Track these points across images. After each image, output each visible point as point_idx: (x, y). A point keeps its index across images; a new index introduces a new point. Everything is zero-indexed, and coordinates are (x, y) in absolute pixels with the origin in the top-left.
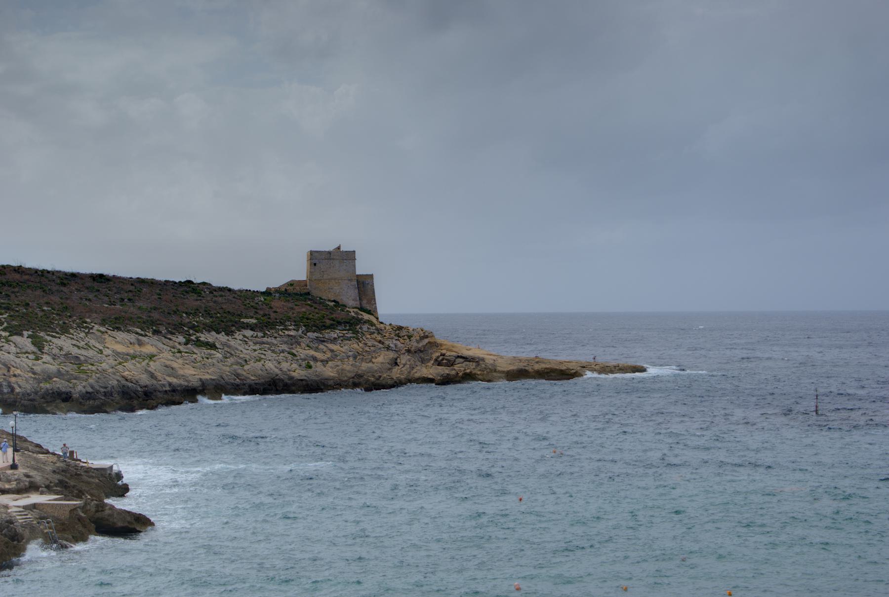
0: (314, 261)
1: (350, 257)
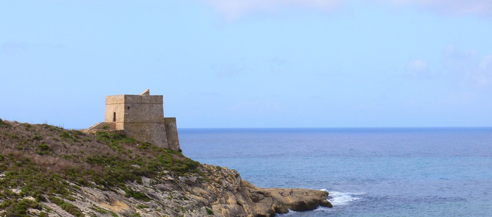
0: (129, 105)
1: (159, 100)
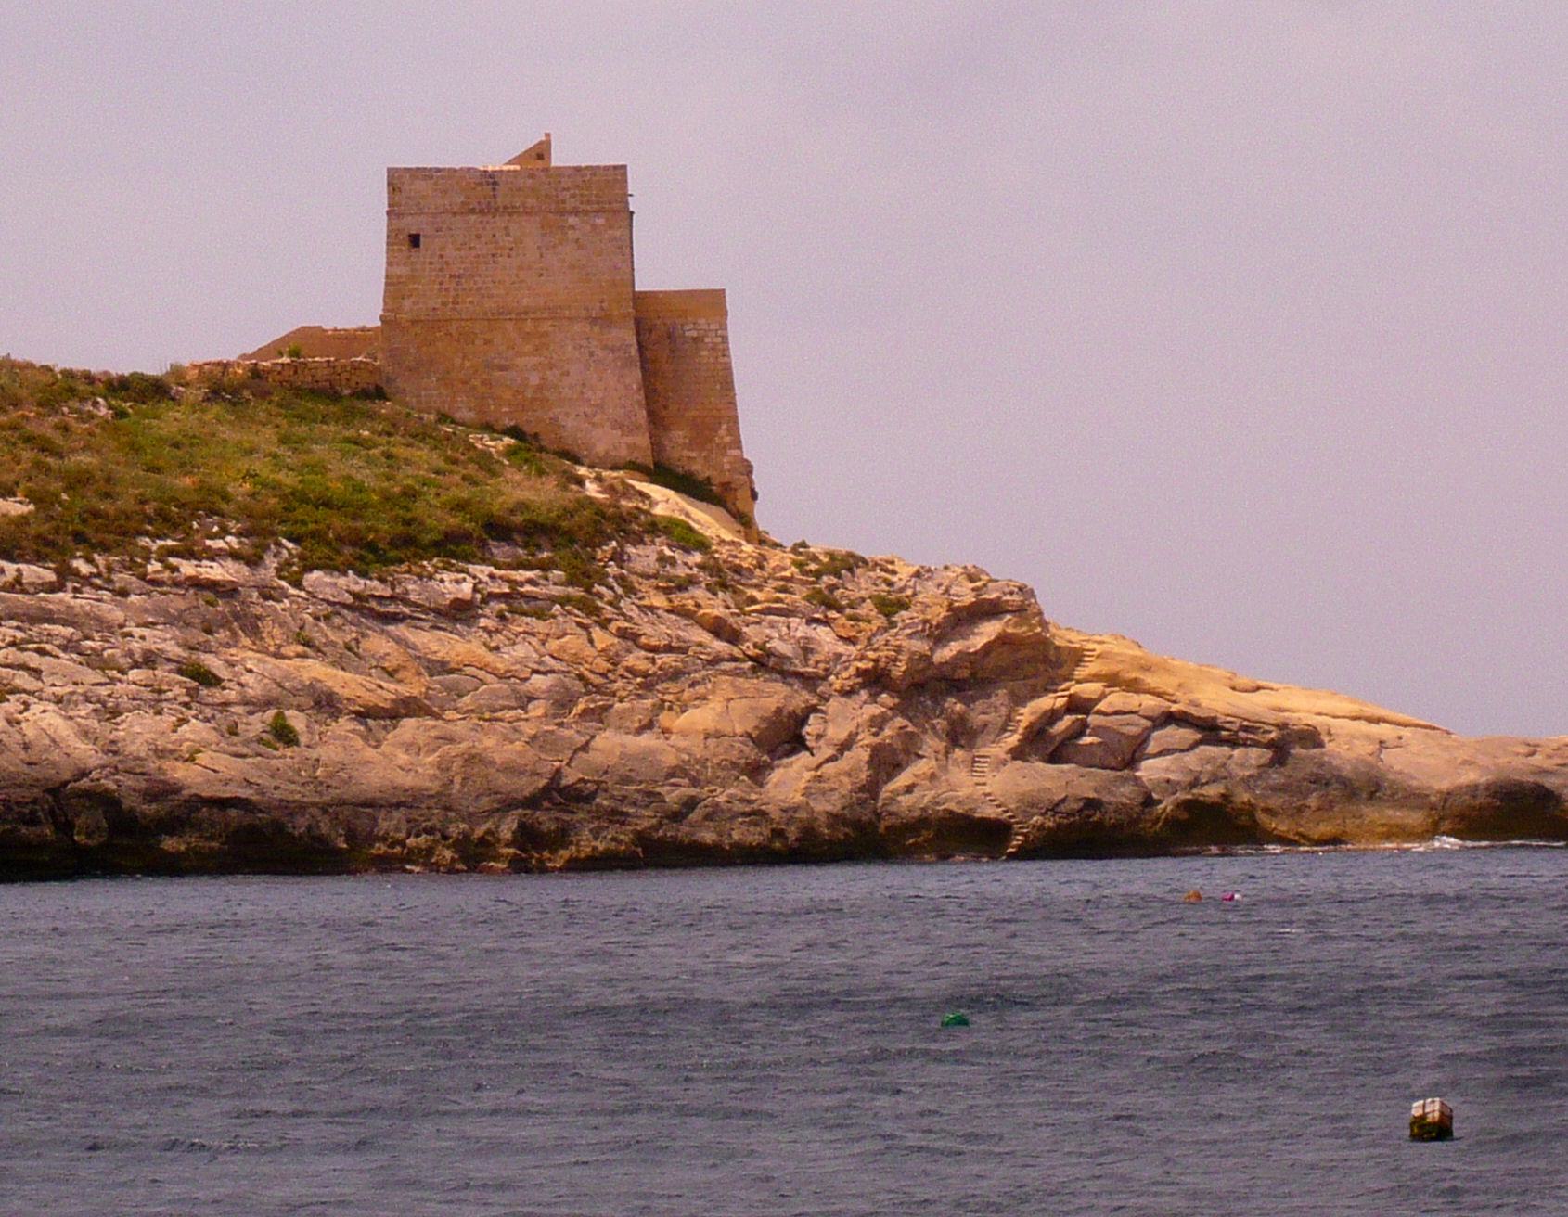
0: (412, 224)
1: (601, 197)
